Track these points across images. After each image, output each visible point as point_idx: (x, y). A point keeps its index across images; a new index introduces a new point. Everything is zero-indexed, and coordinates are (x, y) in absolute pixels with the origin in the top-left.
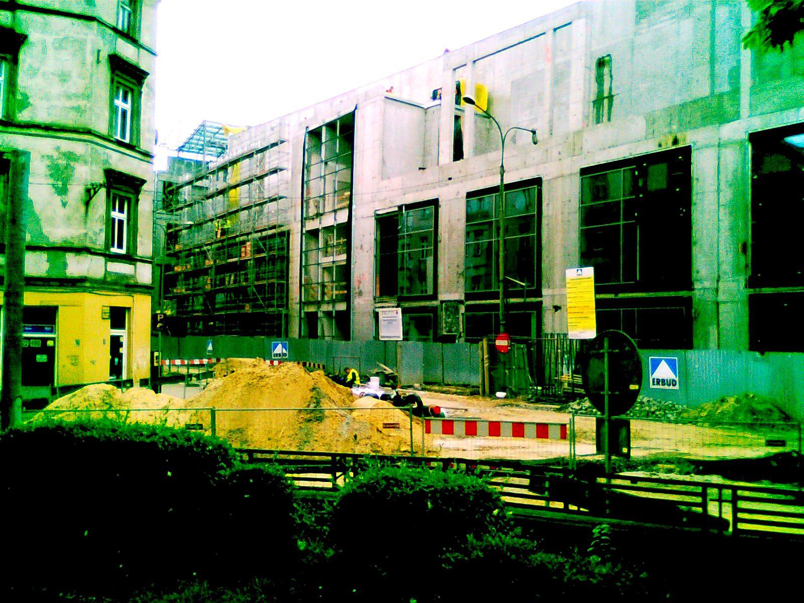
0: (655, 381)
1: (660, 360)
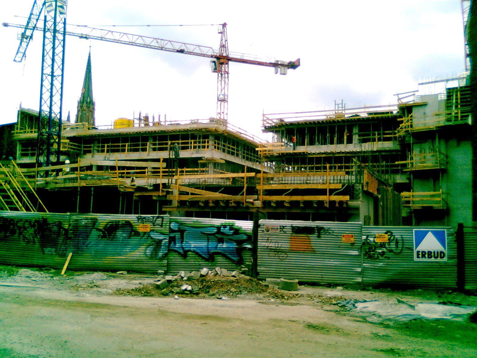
0: (420, 253)
1: (426, 233)
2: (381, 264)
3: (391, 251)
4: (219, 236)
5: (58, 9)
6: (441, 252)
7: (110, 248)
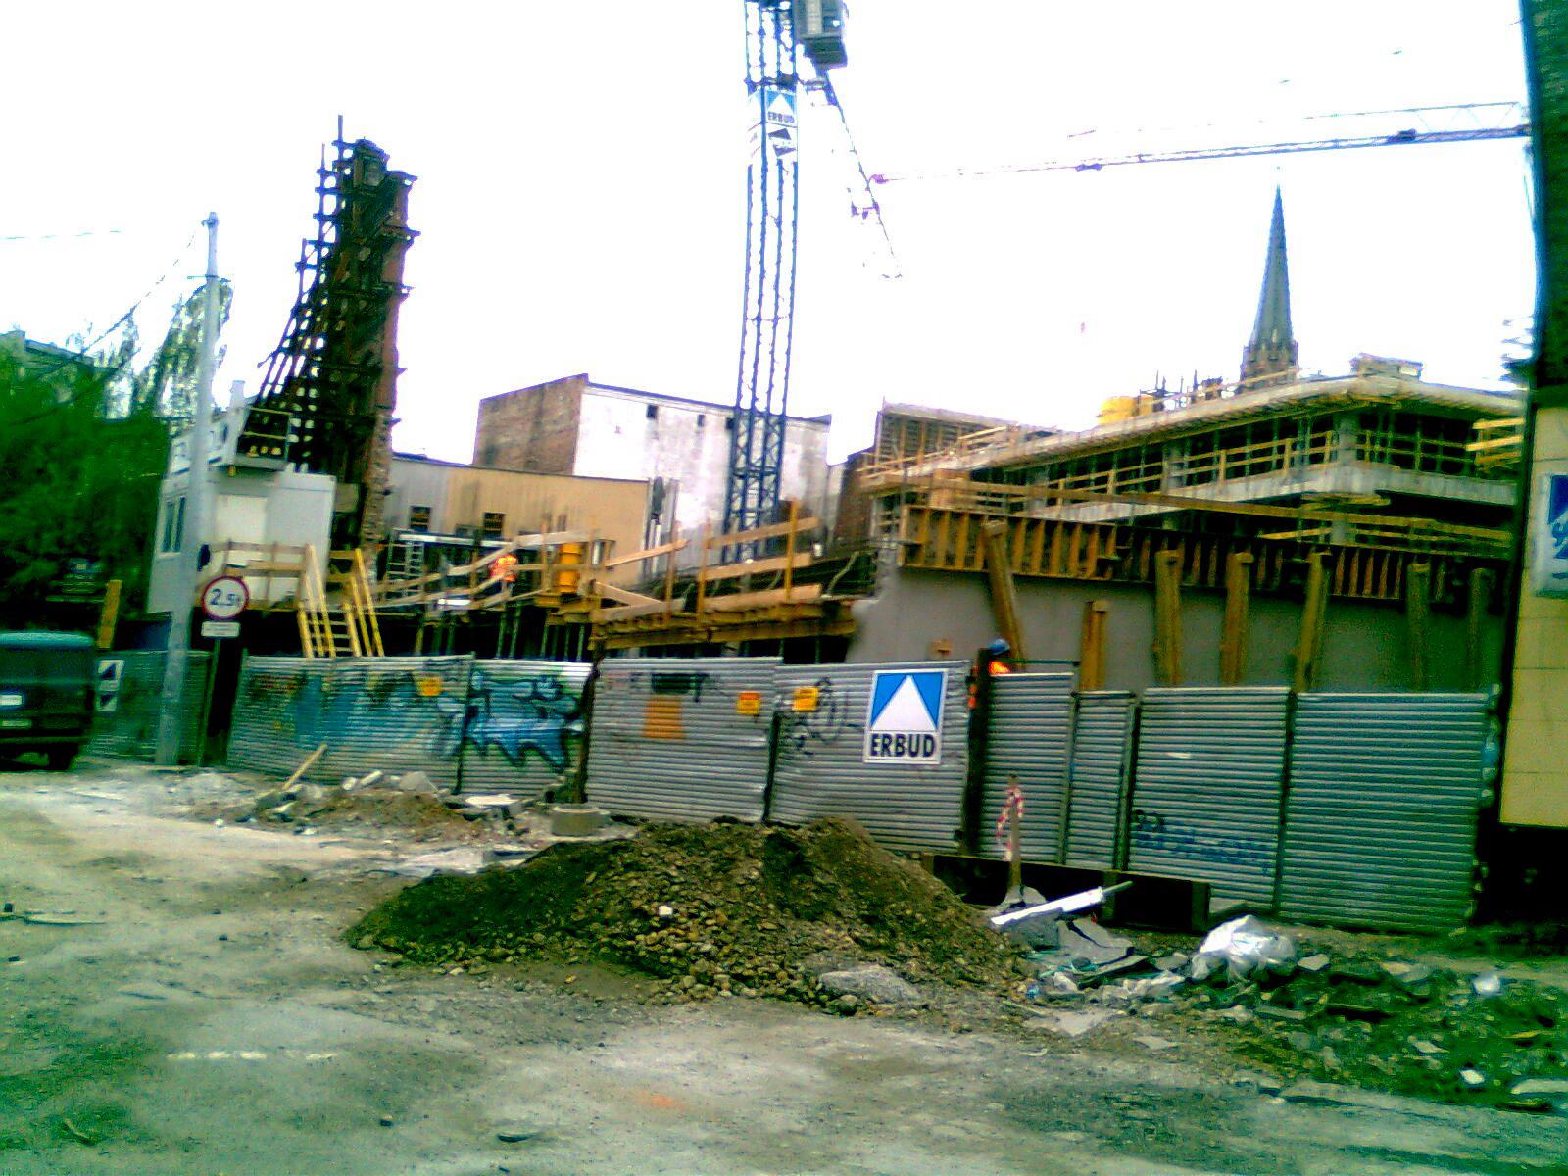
2: (798, 770)
3: (816, 735)
4: (539, 703)
5: (771, 142)
6: (928, 737)
7: (378, 734)
